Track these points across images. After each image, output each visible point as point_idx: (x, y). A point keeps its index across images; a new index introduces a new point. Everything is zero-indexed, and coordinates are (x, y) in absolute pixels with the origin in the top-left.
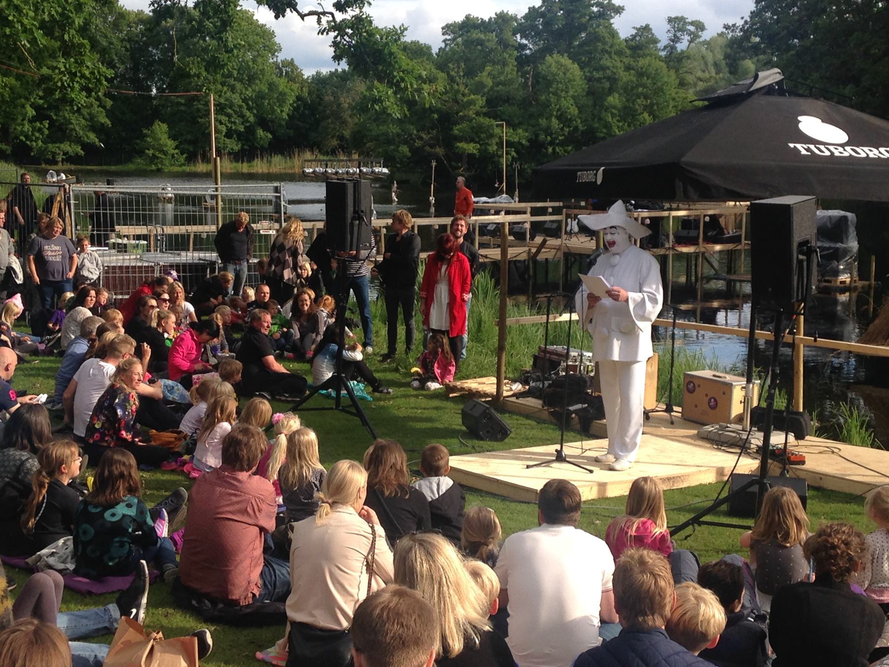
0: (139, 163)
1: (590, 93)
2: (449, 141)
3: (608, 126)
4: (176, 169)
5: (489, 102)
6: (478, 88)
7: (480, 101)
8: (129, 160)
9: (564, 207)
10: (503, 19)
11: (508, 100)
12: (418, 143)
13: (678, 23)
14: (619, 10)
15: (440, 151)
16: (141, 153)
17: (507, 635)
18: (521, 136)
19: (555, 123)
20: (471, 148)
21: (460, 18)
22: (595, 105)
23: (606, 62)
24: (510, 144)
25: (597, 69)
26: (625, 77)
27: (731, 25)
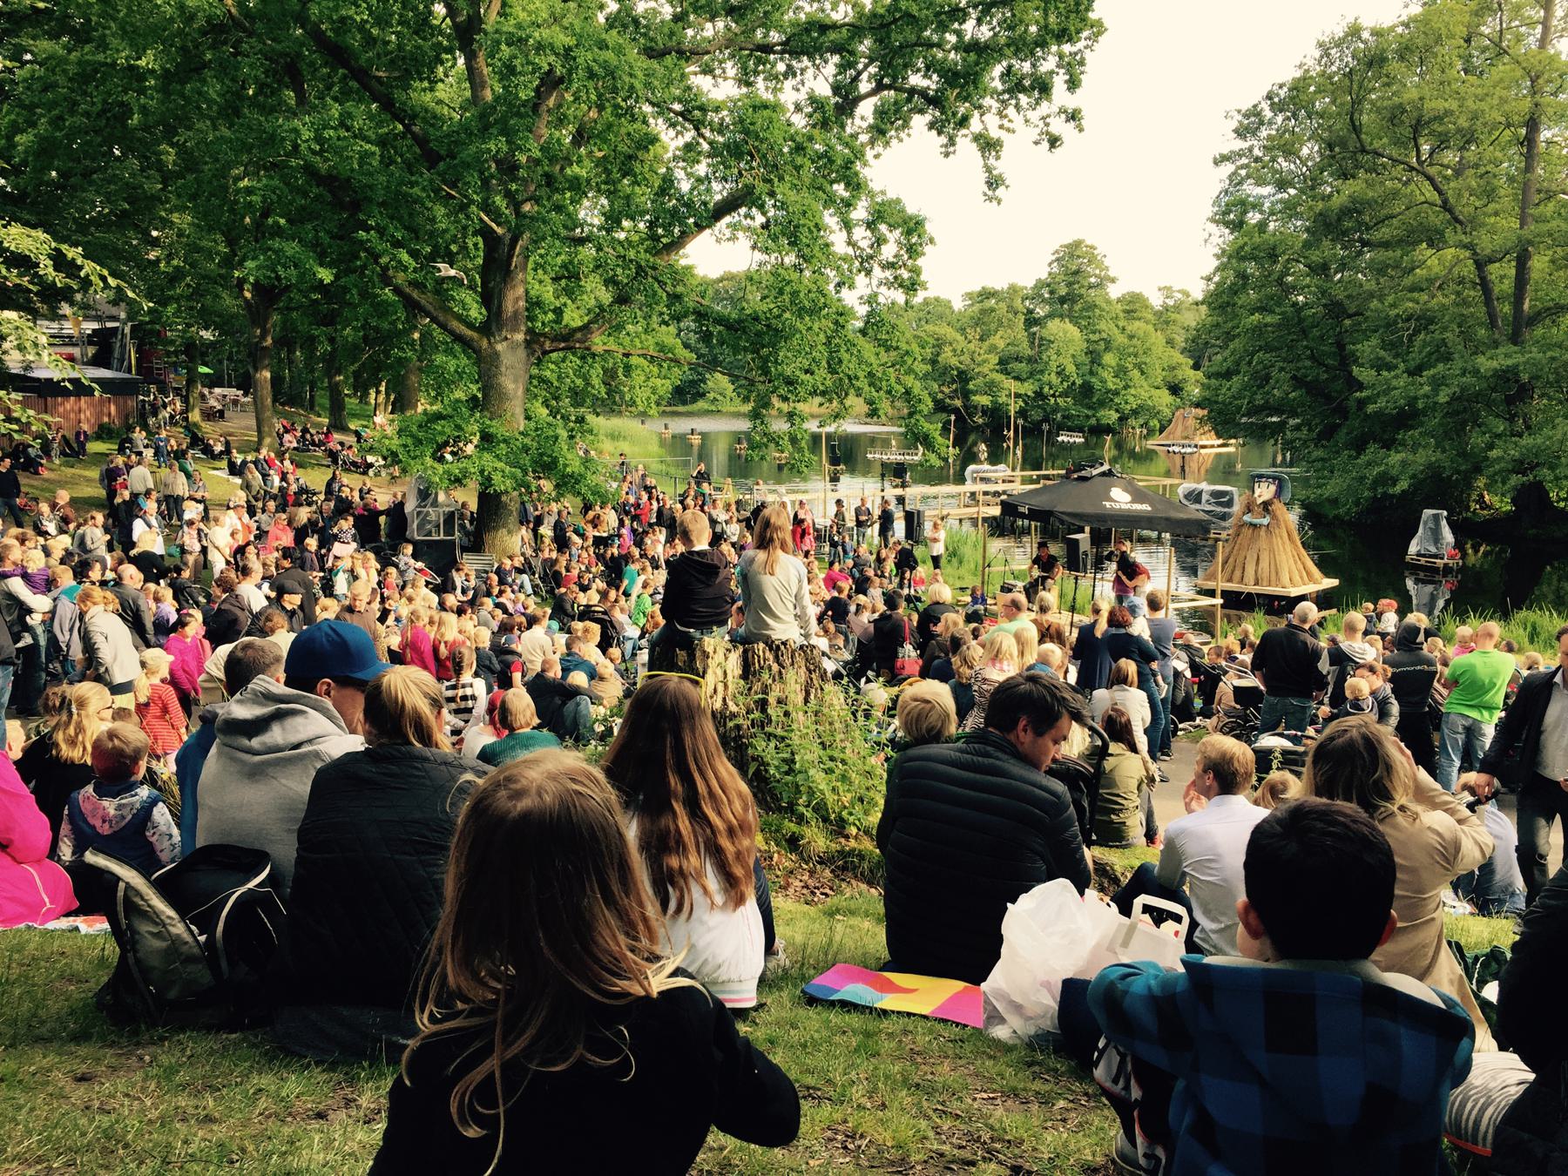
0: (701, 404)
1: (1089, 352)
2: (966, 394)
3: (1104, 381)
4: (733, 409)
5: (1001, 362)
6: (992, 349)
7: (994, 359)
8: (694, 401)
9: (1304, 630)
10: (1013, 289)
11: (1018, 359)
12: (940, 396)
13: (1167, 291)
14: (1113, 281)
15: (958, 403)
16: (703, 395)
17: (1014, 901)
18: (1028, 388)
19: (1055, 379)
20: (984, 400)
21: (978, 289)
22: (1092, 362)
23: (1102, 325)
24: (1018, 396)
25: (1094, 332)
26: (1121, 339)
27: (920, 262)
